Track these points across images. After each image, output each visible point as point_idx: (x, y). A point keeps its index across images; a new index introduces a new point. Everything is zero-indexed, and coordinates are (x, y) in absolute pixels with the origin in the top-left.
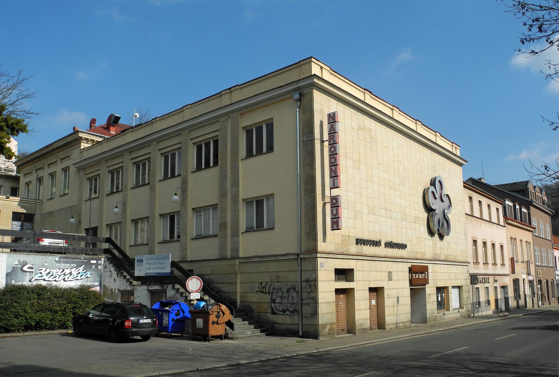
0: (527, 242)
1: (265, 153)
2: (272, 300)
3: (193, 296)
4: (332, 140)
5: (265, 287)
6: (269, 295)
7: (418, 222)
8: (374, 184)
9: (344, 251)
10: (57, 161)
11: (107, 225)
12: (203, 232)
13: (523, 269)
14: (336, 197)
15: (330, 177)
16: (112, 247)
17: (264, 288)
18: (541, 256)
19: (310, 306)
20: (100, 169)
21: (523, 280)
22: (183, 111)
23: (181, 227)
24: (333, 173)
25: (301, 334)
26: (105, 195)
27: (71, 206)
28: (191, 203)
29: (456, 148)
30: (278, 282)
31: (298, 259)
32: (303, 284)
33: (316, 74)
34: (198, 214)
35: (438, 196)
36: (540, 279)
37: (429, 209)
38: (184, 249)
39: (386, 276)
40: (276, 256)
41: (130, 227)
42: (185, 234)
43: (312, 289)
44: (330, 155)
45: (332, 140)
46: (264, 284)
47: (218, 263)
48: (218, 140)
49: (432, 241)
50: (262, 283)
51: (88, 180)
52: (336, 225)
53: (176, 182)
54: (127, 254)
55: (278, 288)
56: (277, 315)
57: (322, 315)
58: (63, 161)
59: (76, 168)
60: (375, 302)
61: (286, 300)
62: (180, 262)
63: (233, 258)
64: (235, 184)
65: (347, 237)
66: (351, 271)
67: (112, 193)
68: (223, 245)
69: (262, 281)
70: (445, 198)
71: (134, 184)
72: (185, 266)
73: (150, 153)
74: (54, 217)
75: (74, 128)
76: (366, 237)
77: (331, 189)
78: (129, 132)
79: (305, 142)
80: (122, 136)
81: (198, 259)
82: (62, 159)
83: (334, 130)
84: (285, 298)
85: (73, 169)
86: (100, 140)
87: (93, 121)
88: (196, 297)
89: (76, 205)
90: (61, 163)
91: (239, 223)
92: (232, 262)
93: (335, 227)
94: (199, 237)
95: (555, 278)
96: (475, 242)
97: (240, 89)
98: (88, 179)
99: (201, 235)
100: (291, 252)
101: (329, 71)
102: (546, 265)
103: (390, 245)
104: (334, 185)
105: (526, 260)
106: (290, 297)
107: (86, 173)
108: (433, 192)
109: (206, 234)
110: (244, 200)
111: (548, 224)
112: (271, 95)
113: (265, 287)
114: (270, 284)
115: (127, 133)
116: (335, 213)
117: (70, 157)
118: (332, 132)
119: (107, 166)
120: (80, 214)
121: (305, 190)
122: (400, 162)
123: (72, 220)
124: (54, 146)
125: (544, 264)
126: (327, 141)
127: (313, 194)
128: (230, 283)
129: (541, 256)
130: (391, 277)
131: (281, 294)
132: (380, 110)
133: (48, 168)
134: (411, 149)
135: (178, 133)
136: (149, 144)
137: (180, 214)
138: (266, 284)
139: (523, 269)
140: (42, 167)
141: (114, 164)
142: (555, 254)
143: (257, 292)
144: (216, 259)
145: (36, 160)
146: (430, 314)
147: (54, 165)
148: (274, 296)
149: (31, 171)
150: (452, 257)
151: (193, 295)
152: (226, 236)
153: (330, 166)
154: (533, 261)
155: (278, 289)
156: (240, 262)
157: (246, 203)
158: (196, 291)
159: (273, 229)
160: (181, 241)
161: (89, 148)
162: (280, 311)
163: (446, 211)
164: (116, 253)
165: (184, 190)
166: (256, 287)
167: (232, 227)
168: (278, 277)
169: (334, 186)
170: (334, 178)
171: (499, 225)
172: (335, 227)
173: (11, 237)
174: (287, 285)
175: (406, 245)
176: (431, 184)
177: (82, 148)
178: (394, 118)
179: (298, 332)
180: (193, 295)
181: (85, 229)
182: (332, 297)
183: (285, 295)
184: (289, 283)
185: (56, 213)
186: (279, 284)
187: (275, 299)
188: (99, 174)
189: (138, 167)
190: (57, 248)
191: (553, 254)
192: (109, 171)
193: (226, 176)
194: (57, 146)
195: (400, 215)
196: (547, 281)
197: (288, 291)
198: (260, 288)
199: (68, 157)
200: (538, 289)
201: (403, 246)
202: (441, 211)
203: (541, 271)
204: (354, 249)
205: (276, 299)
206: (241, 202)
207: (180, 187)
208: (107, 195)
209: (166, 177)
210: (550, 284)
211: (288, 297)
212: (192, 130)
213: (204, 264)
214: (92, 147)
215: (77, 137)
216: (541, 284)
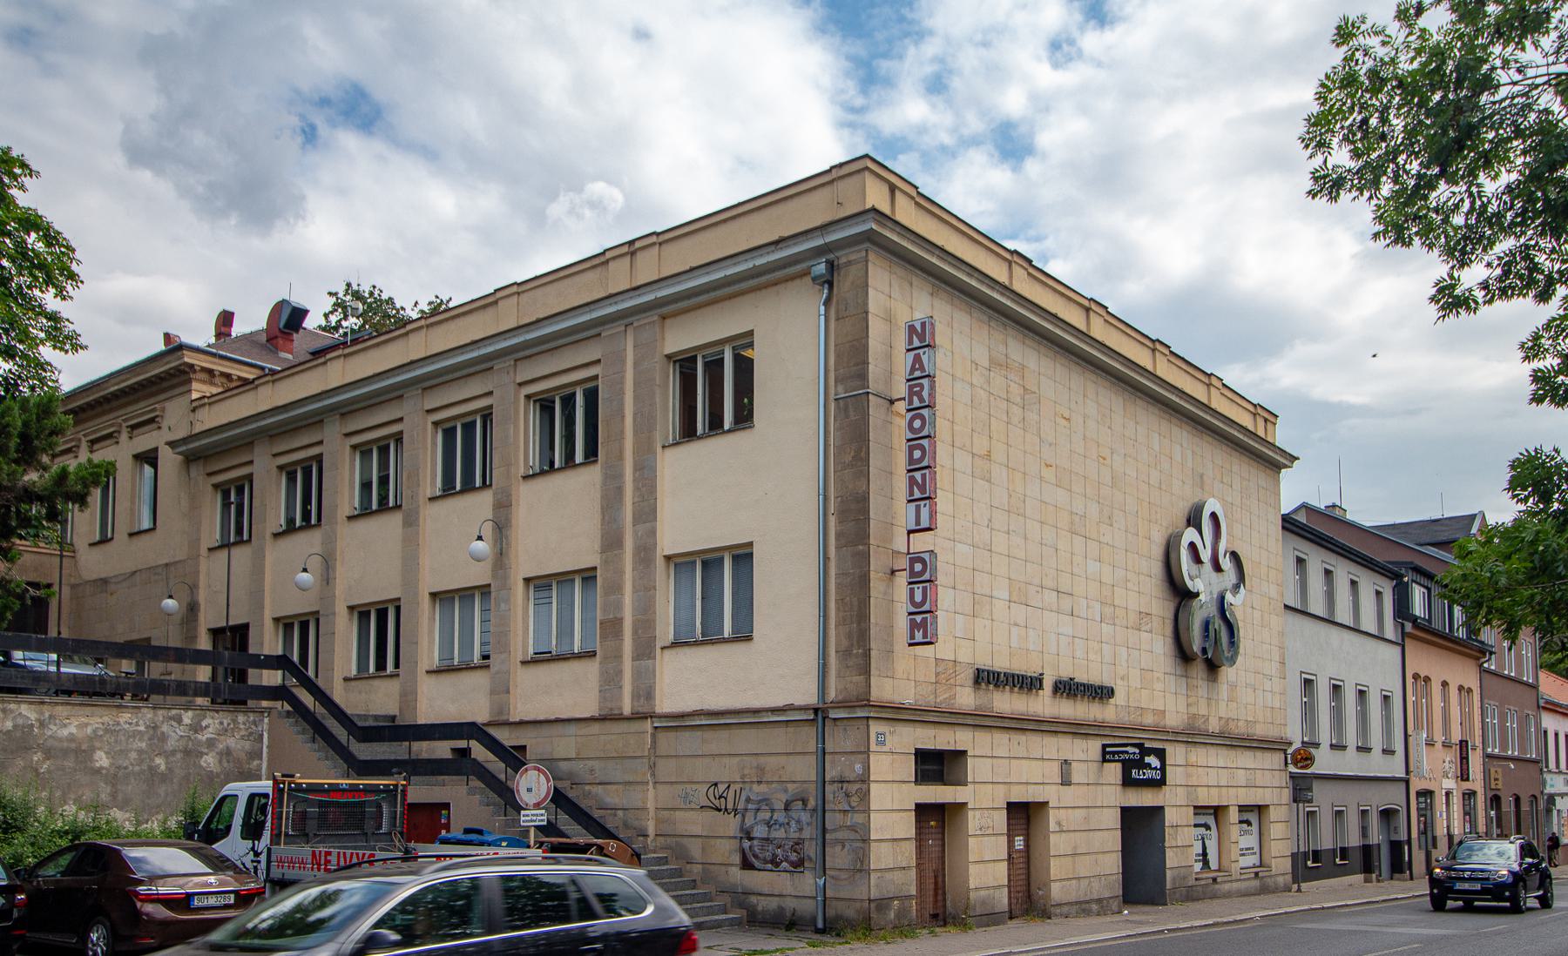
0: (1461, 688)
1: (729, 431)
2: (742, 829)
3: (527, 818)
4: (915, 398)
5: (725, 795)
6: (735, 815)
7: (1148, 628)
8: (1028, 521)
9: (941, 703)
10: (119, 432)
11: (277, 620)
12: (554, 642)
13: (1447, 764)
14: (922, 555)
17: (720, 797)
18: (1503, 729)
19: (846, 849)
21: (1448, 794)
22: (496, 302)
23: (492, 629)
24: (920, 481)
25: (820, 925)
26: (268, 536)
27: (167, 565)
28: (526, 563)
29: (1266, 420)
30: (759, 782)
32: (828, 788)
33: (878, 207)
34: (542, 594)
35: (1206, 555)
36: (1498, 793)
37: (1181, 594)
38: (501, 689)
39: (1054, 771)
40: (756, 712)
42: (505, 648)
43: (854, 804)
45: (915, 398)
46: (722, 788)
47: (595, 728)
50: (716, 784)
51: (216, 491)
52: (922, 627)
53: (480, 505)
55: (760, 798)
56: (756, 872)
57: (879, 874)
58: (135, 432)
59: (179, 453)
60: (1022, 843)
61: (783, 830)
62: (489, 724)
63: (638, 717)
64: (647, 514)
65: (951, 664)
66: (961, 755)
67: (291, 528)
68: (610, 680)
69: (716, 780)
70: (1226, 563)
71: (357, 505)
72: (506, 737)
73: (401, 419)
74: (112, 594)
75: (167, 337)
76: (1001, 664)
77: (909, 532)
78: (339, 357)
81: (542, 718)
82: (133, 427)
84: (777, 826)
85: (169, 460)
86: (251, 377)
87: (226, 319)
89: (180, 561)
90: (131, 438)
91: (654, 621)
92: (635, 726)
93: (919, 637)
94: (541, 658)
95: (1542, 792)
96: (1308, 683)
97: (660, 244)
98: (216, 486)
99: (550, 652)
100: (797, 703)
101: (913, 198)
102: (1516, 753)
103: (1067, 688)
104: (918, 522)
105: (1456, 737)
106: (793, 824)
108: (1192, 546)
109: (565, 649)
110: (668, 558)
111: (1528, 639)
112: (750, 265)
113: (725, 795)
114: (737, 787)
115: (330, 359)
117: (158, 422)
118: (917, 374)
120: (193, 588)
121: (839, 535)
122: (1104, 459)
123: (170, 603)
124: (106, 389)
125: (1510, 752)
126: (904, 399)
127: (861, 547)
128: (630, 783)
129: (1503, 729)
130: (1069, 774)
131: (767, 815)
132: (1053, 311)
134: (1137, 423)
135: (483, 366)
137: (490, 593)
138: (729, 787)
139: (1447, 764)
140: (71, 448)
141: (297, 448)
142: (1544, 725)
143: (702, 807)
146: (1174, 879)
147: (108, 442)
148: (749, 821)
149: (73, 444)
150: (1241, 724)
151: (528, 815)
152: (618, 656)
154: (1478, 742)
155: (760, 802)
156: (656, 728)
157: (675, 565)
158: (537, 806)
159: (749, 638)
160: (493, 669)
162: (766, 862)
163: (1229, 597)
165: (501, 527)
166: (700, 794)
167: (635, 632)
168: (761, 769)
170: (918, 503)
171: (1380, 638)
172: (919, 637)
174: (786, 791)
175: (1112, 689)
176: (1189, 523)
177: (195, 395)
178: (1092, 334)
179: (814, 919)
180: (528, 815)
181: (209, 630)
182: (906, 826)
183: (780, 816)
184: (790, 787)
185: (119, 582)
186: (763, 788)
187: (752, 827)
190: (128, 684)
191: (1538, 723)
192: (281, 468)
193: (620, 490)
194: (116, 388)
195: (1097, 606)
196: (1517, 800)
197: (787, 808)
198: (712, 798)
199: (152, 421)
200: (1488, 818)
201: (1105, 691)
202: (1215, 596)
203: (1499, 770)
204: (966, 698)
205: (755, 829)
206: (660, 562)
208: (276, 535)
209: (448, 490)
210: (1525, 807)
211: (788, 824)
213: (558, 729)
215: (180, 365)
216: (1498, 808)
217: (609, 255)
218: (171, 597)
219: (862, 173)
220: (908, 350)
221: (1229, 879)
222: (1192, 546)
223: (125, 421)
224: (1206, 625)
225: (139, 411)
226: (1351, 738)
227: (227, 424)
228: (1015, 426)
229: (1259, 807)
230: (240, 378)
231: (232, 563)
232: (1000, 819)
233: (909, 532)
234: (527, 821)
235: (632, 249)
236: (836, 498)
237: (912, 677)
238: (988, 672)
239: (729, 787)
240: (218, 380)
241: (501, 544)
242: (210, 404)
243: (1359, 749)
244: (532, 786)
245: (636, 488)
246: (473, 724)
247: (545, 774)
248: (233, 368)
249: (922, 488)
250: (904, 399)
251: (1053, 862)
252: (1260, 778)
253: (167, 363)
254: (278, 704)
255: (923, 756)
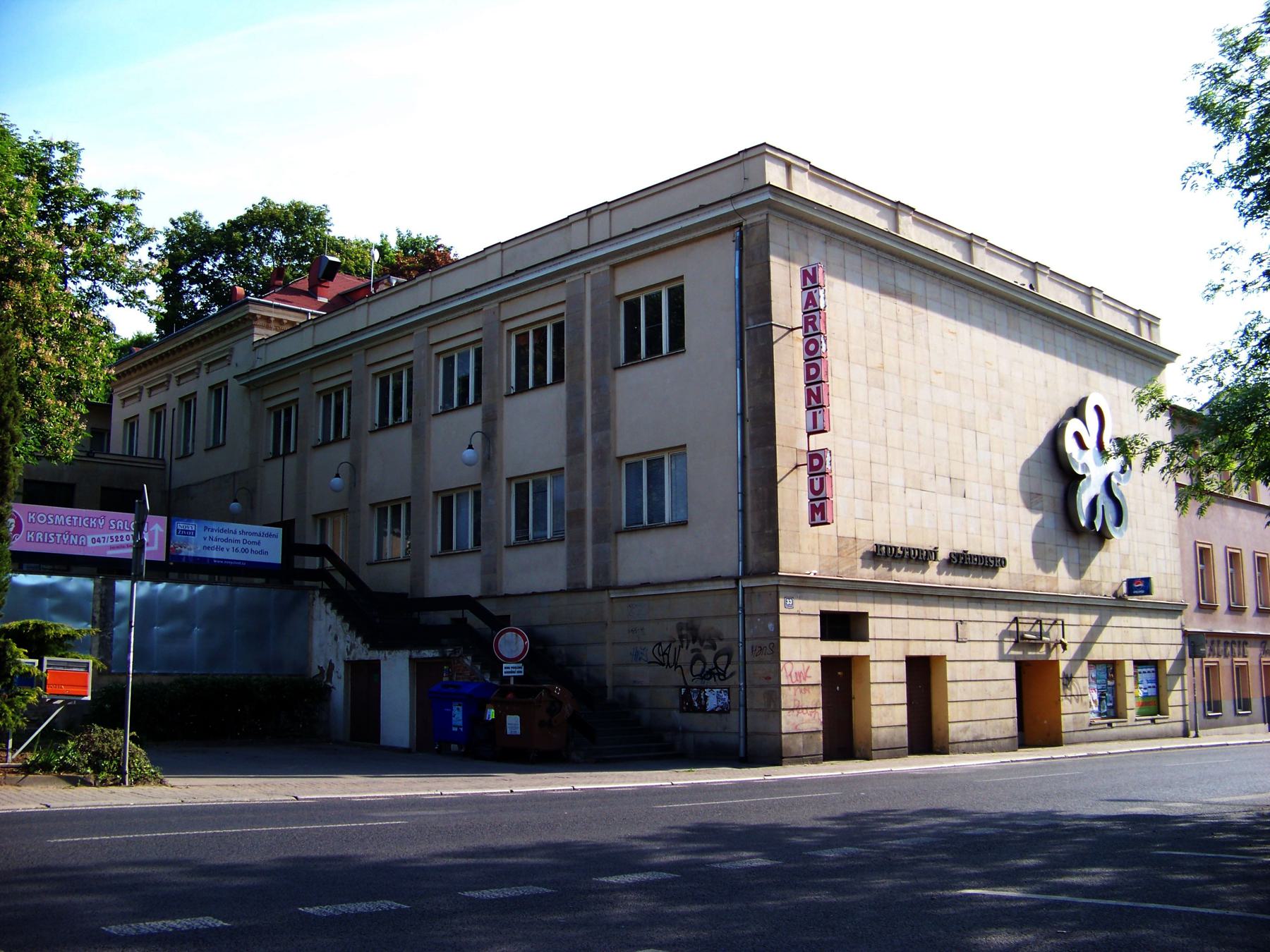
5: (667, 652)
11: (315, 516)
15: (808, 409)
16: (328, 564)
17: (664, 654)
20: (297, 389)
25: (742, 754)
27: (234, 474)
31: (737, 589)
38: (491, 569)
39: (948, 630)
41: (369, 522)
44: (806, 360)
46: (665, 646)
48: (563, 323)
49: (1077, 550)
50: (660, 644)
52: (819, 512)
54: (361, 577)
62: (480, 597)
64: (604, 422)
65: (851, 542)
67: (326, 443)
68: (575, 560)
69: (659, 640)
71: (377, 422)
77: (809, 434)
79: (751, 331)
80: (348, 311)
83: (815, 304)
85: (235, 387)
88: (514, 672)
92: (595, 597)
97: (611, 210)
103: (960, 561)
104: (815, 425)
107: (266, 396)
108: (1077, 436)
113: (667, 652)
116: (817, 487)
118: (811, 308)
119: (264, 398)
121: (752, 438)
126: (801, 327)
127: (770, 447)
133: (178, 385)
136: (347, 353)
138: (670, 645)
140: (193, 370)
143: (650, 663)
144: (562, 591)
145: (149, 367)
149: (227, 353)
151: (508, 668)
152: (581, 540)
153: (807, 385)
159: (684, 523)
161: (273, 339)
164: (340, 578)
165: (490, 434)
167: (594, 520)
169: (816, 429)
172: (818, 518)
173: (411, 659)
175: (1005, 560)
177: (256, 338)
180: (508, 668)
188: (297, 400)
189: (327, 400)
193: (581, 406)
194: (198, 335)
207: (480, 428)
208: (316, 447)
212: (505, 301)
214: (282, 336)
217: (571, 220)
218: (235, 501)
219: (761, 157)
220: (804, 290)
221: (1125, 724)
222: (1077, 436)
223: (174, 372)
224: (1093, 503)
225: (216, 348)
226: (1222, 601)
227: (280, 361)
228: (906, 342)
229: (1156, 661)
230: (289, 322)
231: (917, 621)
232: (901, 670)
233: (809, 434)
234: (508, 672)
235: (589, 215)
236: (750, 408)
237: (816, 552)
238: (886, 547)
239: (670, 645)
240: (273, 325)
241: (489, 450)
242: (267, 344)
243: (1200, 607)
244: (512, 644)
245: (594, 404)
246: (468, 597)
247: (522, 635)
248: (284, 314)
249: (818, 399)
250: (801, 327)
251: (950, 706)
252: (1154, 636)
253: (237, 314)
254: (319, 584)
255: (826, 617)
